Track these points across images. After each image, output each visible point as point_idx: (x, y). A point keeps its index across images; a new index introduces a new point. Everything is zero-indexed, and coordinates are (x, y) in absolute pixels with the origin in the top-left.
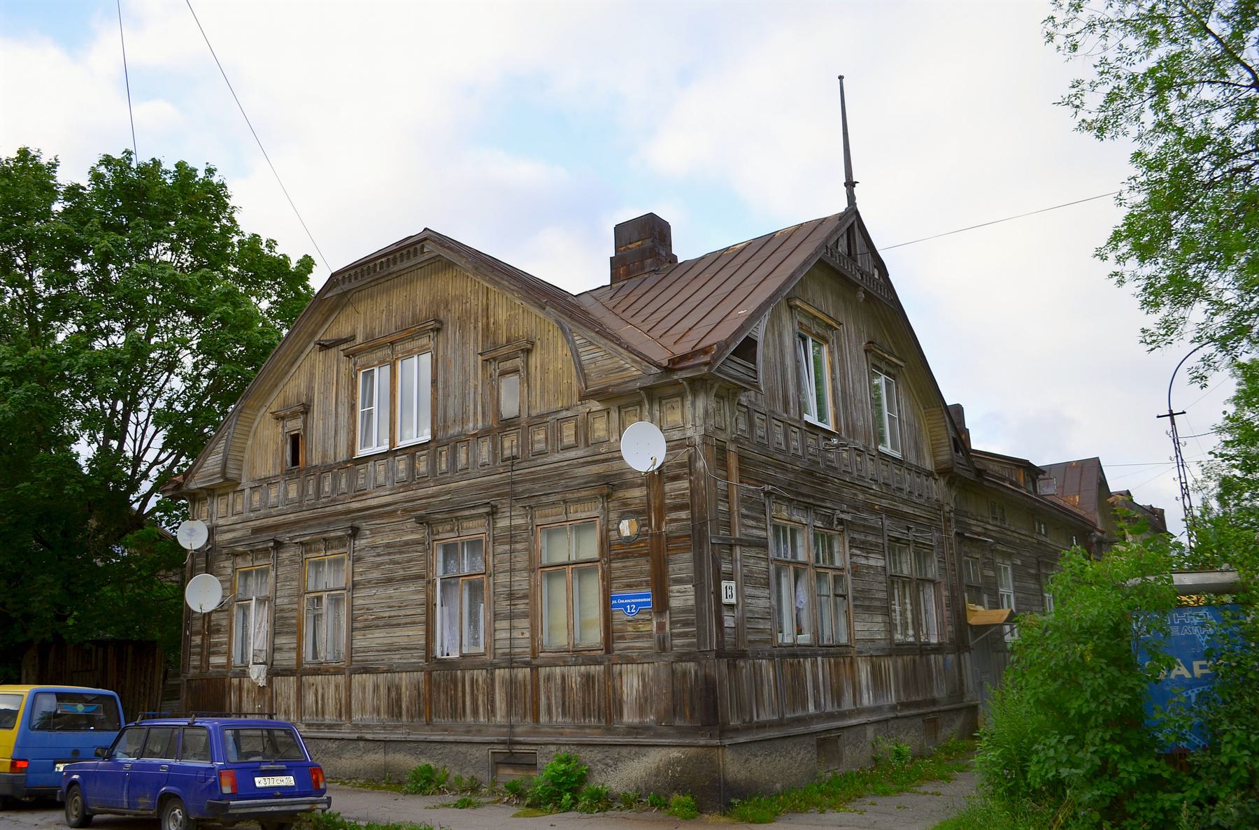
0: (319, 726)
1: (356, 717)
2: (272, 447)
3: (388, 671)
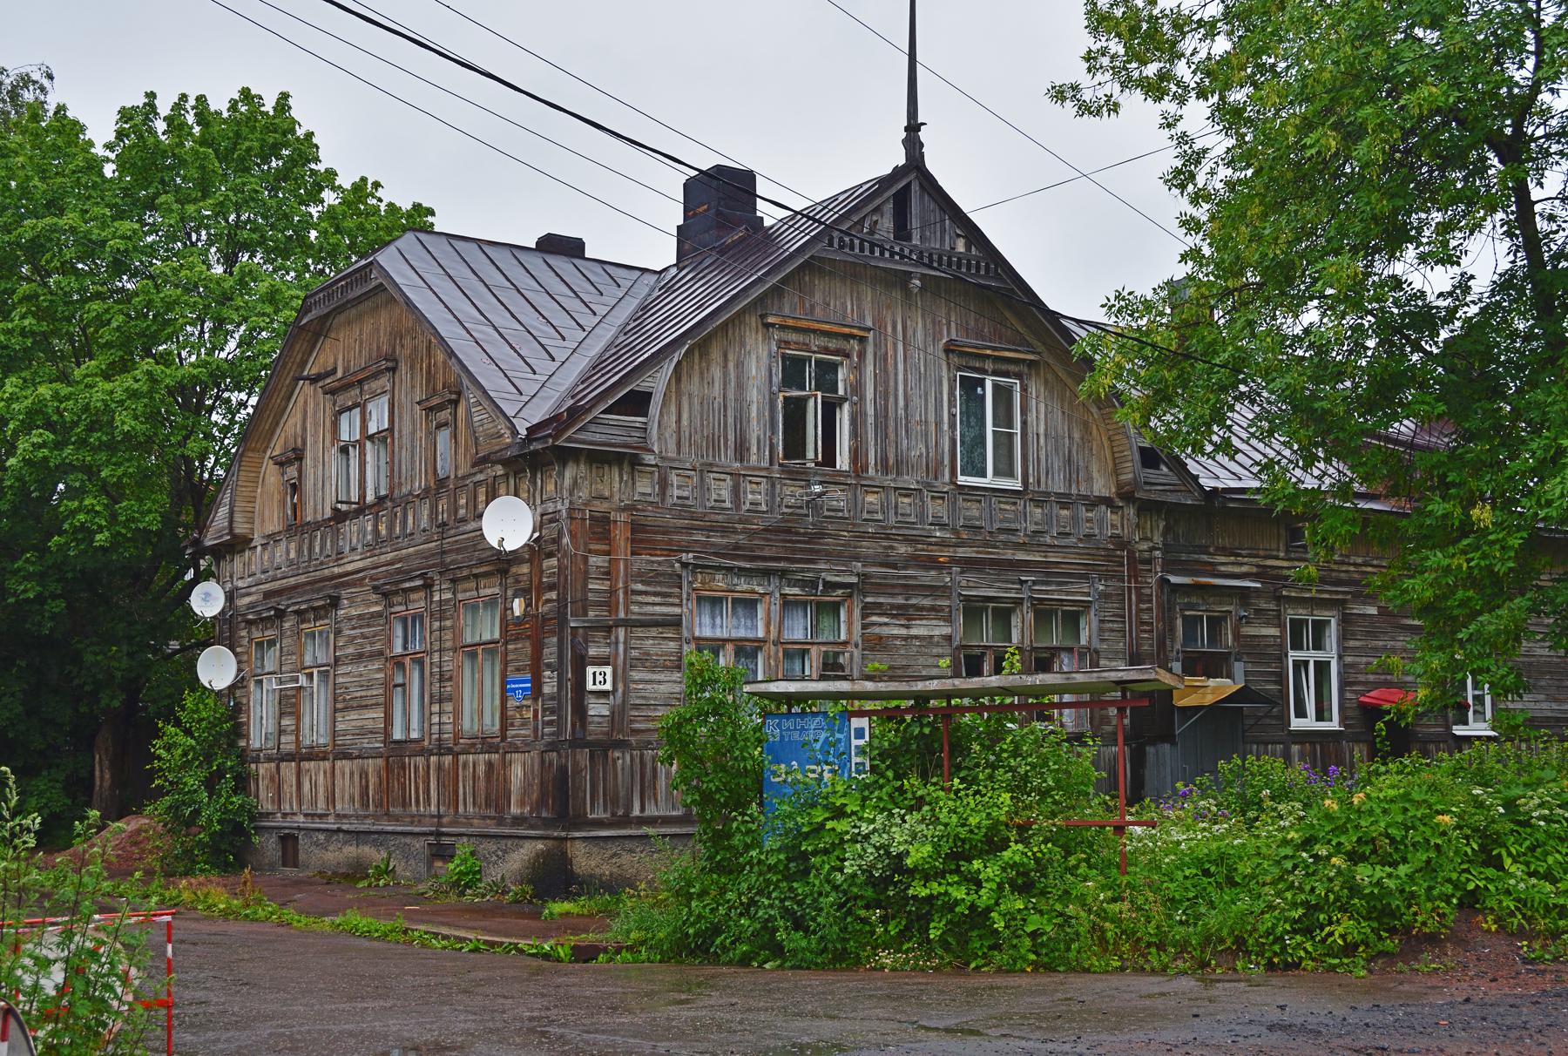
0: (313, 815)
1: (339, 807)
2: (276, 497)
3: (358, 757)
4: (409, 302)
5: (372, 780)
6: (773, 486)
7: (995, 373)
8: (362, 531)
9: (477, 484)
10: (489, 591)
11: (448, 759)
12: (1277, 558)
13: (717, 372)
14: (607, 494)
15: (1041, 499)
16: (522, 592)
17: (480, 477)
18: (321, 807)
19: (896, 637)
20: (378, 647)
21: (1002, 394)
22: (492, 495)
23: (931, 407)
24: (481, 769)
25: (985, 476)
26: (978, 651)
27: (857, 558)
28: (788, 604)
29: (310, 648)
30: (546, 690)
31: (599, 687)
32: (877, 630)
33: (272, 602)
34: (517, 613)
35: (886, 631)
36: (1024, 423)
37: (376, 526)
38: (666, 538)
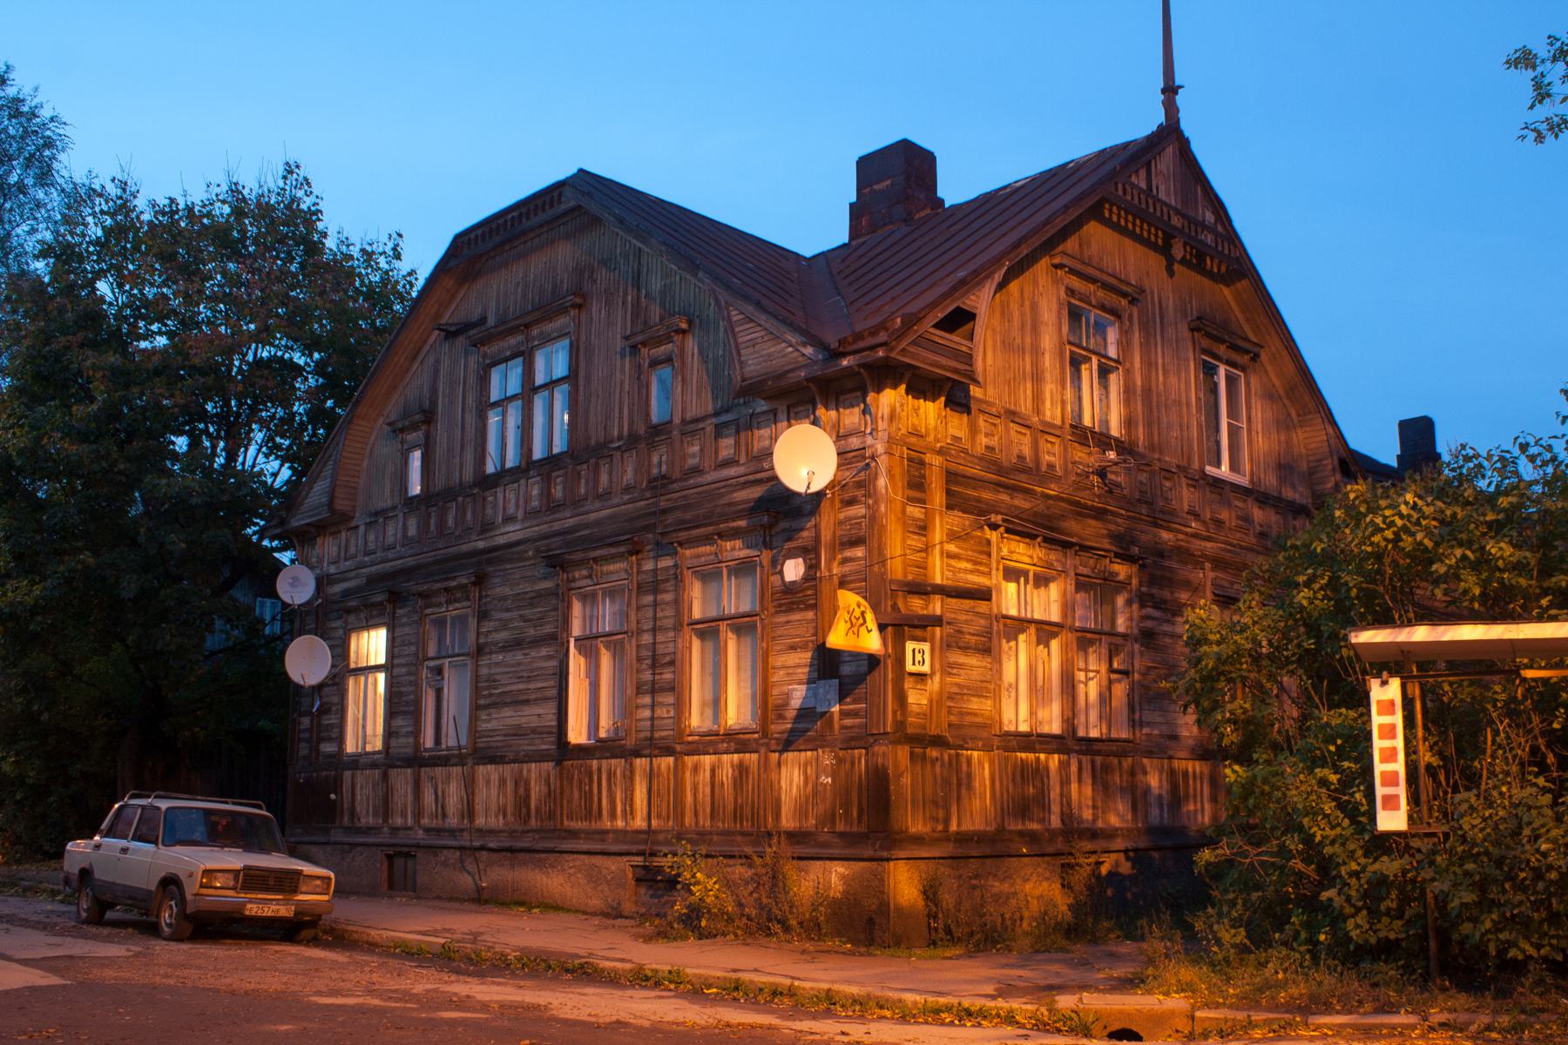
3: (514, 761)
18: (453, 821)
20: (548, 629)
21: (1231, 381)
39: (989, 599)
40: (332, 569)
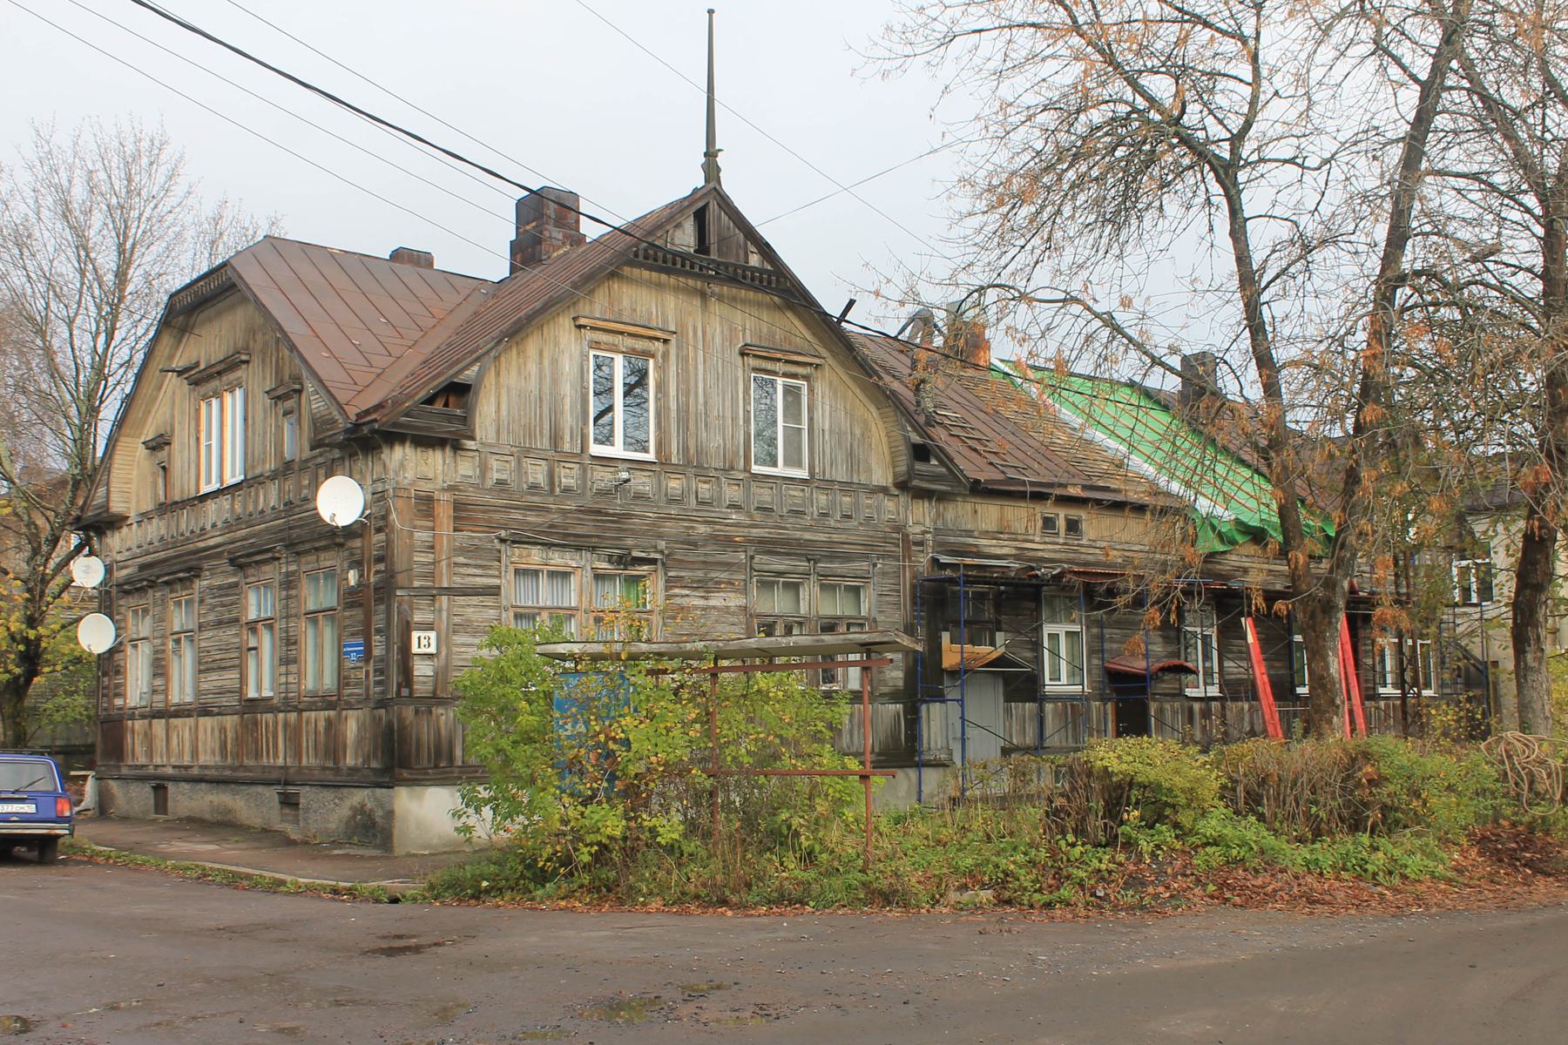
3: (219, 714)
4: (257, 301)
5: (230, 735)
6: (585, 471)
7: (785, 375)
8: (219, 510)
9: (319, 466)
10: (328, 563)
11: (293, 716)
12: (1032, 541)
13: (532, 367)
14: (431, 476)
15: (827, 485)
16: (357, 564)
17: (320, 460)
18: (187, 761)
19: (696, 608)
22: (330, 474)
23: (728, 404)
24: (322, 725)
25: (775, 464)
26: (771, 619)
27: (660, 537)
28: (599, 577)
29: (176, 614)
30: (377, 652)
31: (423, 650)
32: (678, 601)
33: (145, 574)
34: (352, 583)
35: (685, 601)
36: (811, 419)
37: (232, 505)
38: (486, 516)
39: (498, 595)
40: (119, 558)
